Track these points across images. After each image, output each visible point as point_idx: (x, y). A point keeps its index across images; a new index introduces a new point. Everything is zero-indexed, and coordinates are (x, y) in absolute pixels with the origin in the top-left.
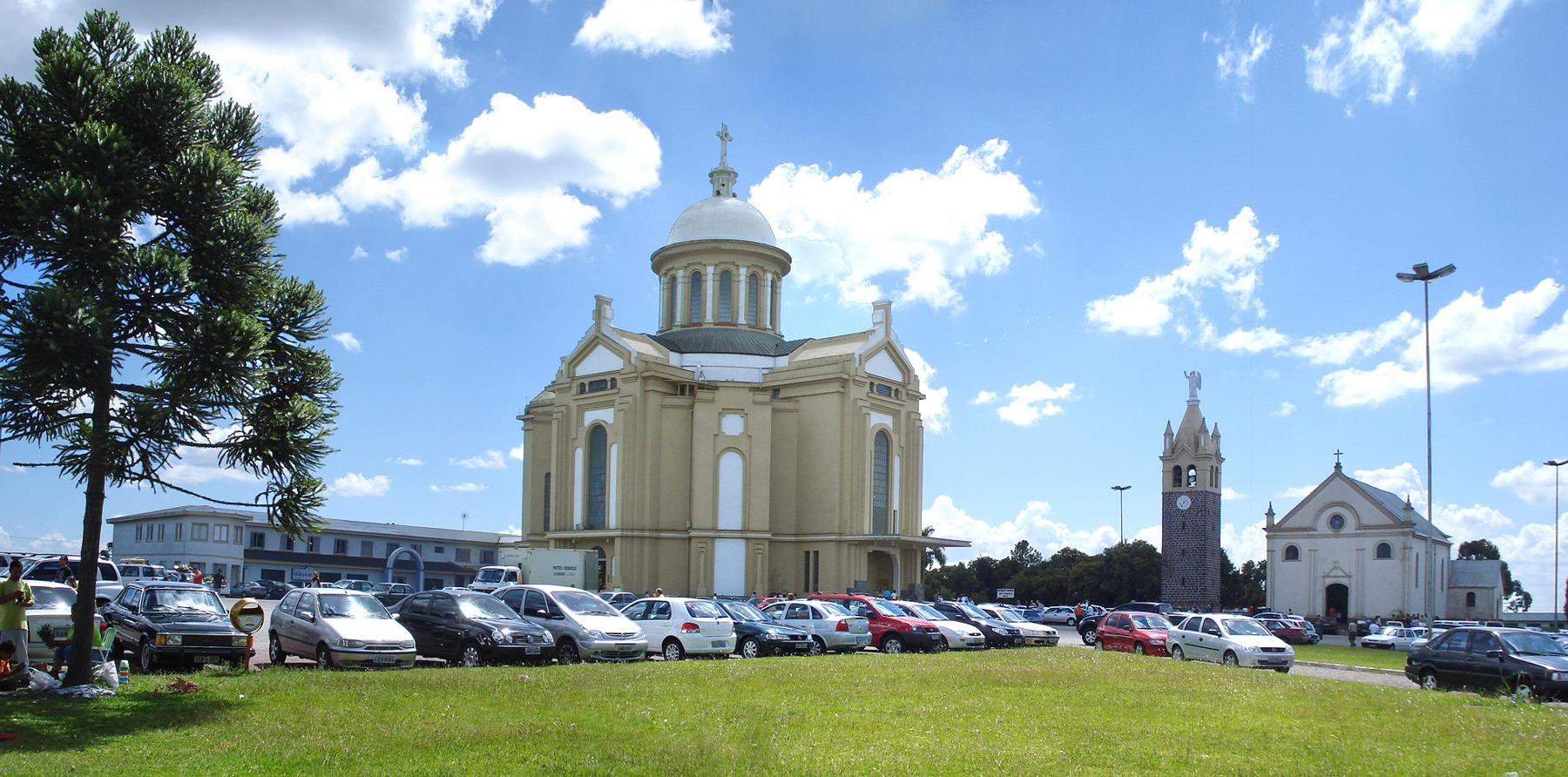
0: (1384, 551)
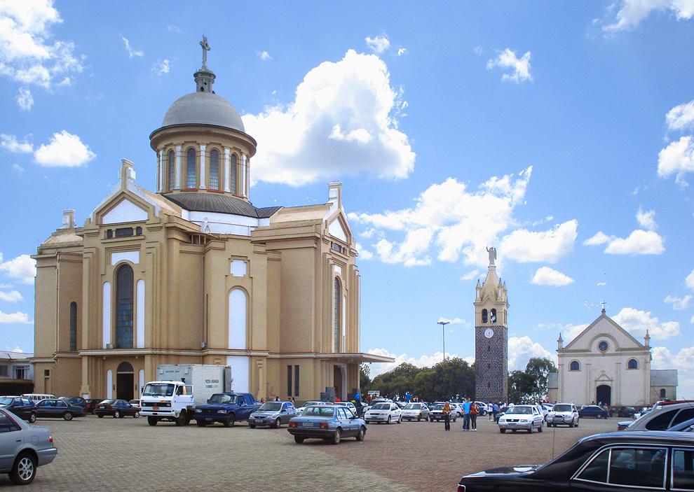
0: (633, 365)
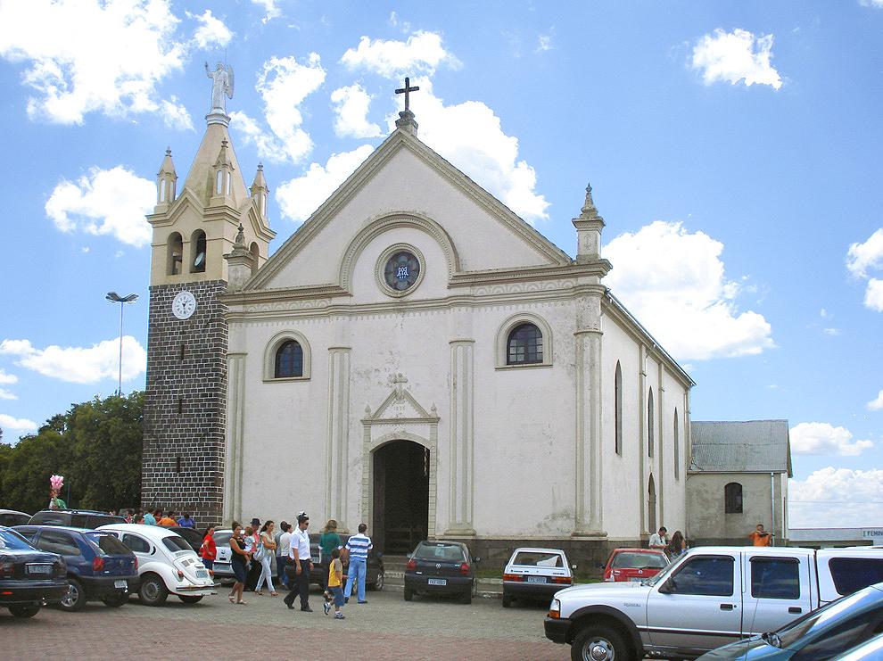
0: (523, 343)
